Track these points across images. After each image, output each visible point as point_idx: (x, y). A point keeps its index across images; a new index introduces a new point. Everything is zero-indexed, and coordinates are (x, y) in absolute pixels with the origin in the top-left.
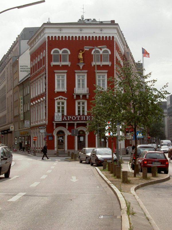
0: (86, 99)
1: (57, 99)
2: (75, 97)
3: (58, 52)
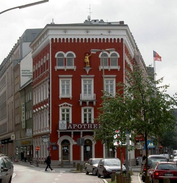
0: (93, 106)
1: (61, 106)
2: (81, 103)
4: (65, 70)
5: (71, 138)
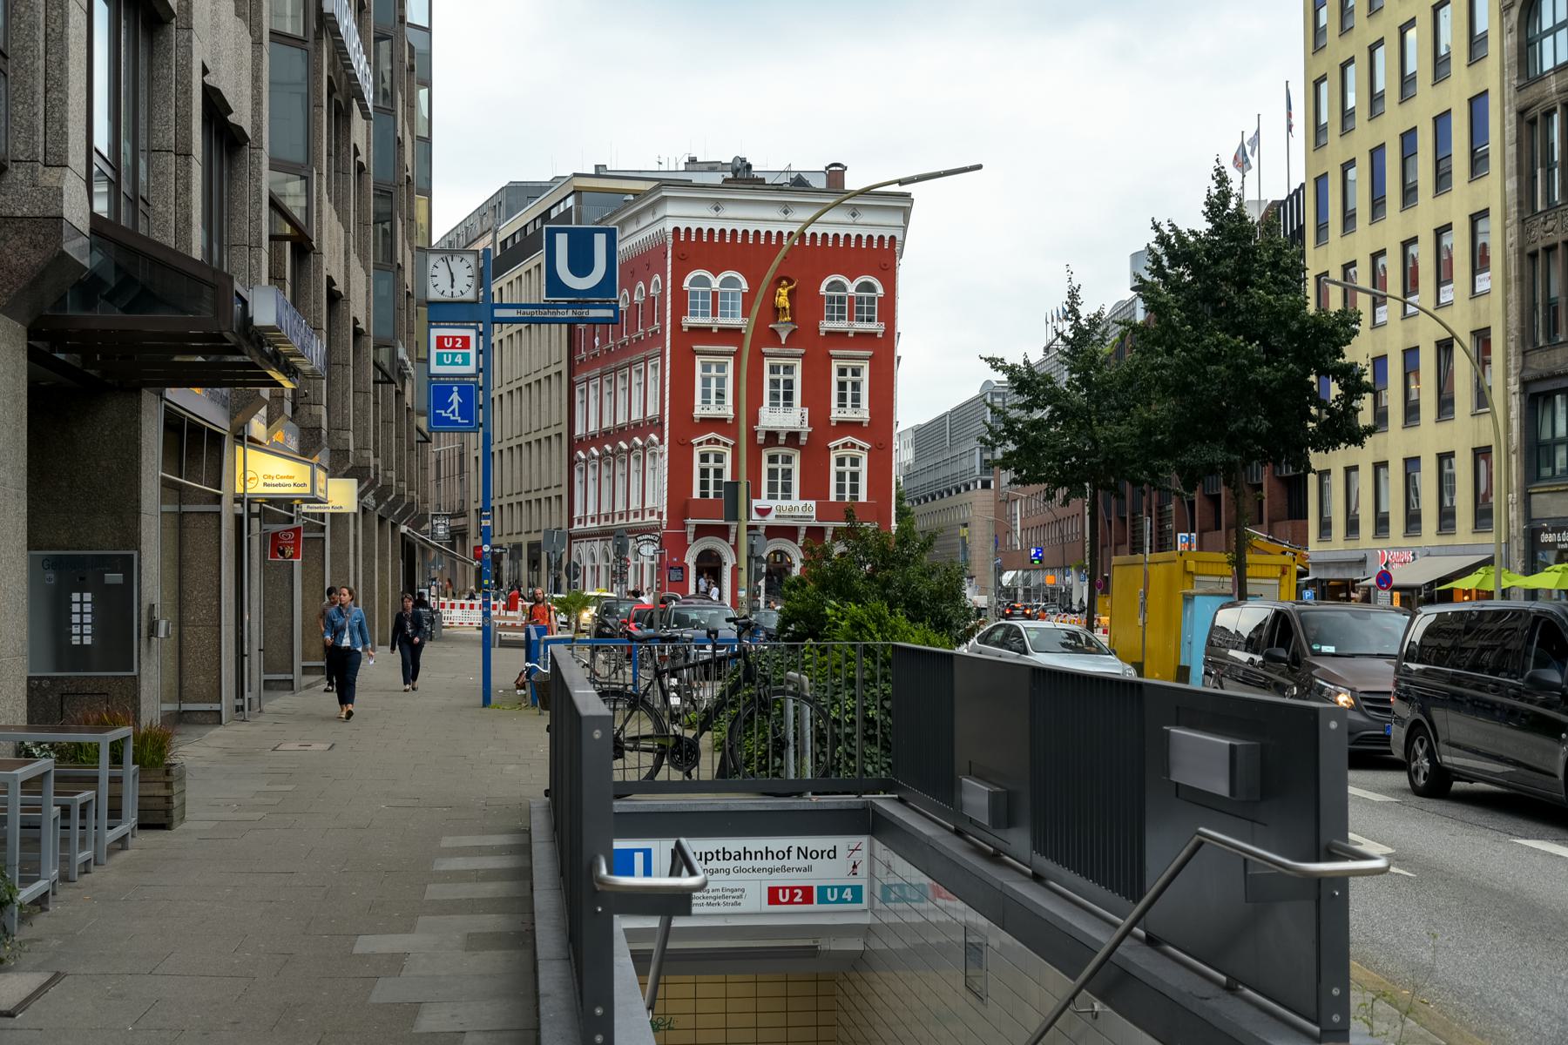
1: (700, 444)
3: (707, 283)
4: (851, 335)
5: (728, 545)
